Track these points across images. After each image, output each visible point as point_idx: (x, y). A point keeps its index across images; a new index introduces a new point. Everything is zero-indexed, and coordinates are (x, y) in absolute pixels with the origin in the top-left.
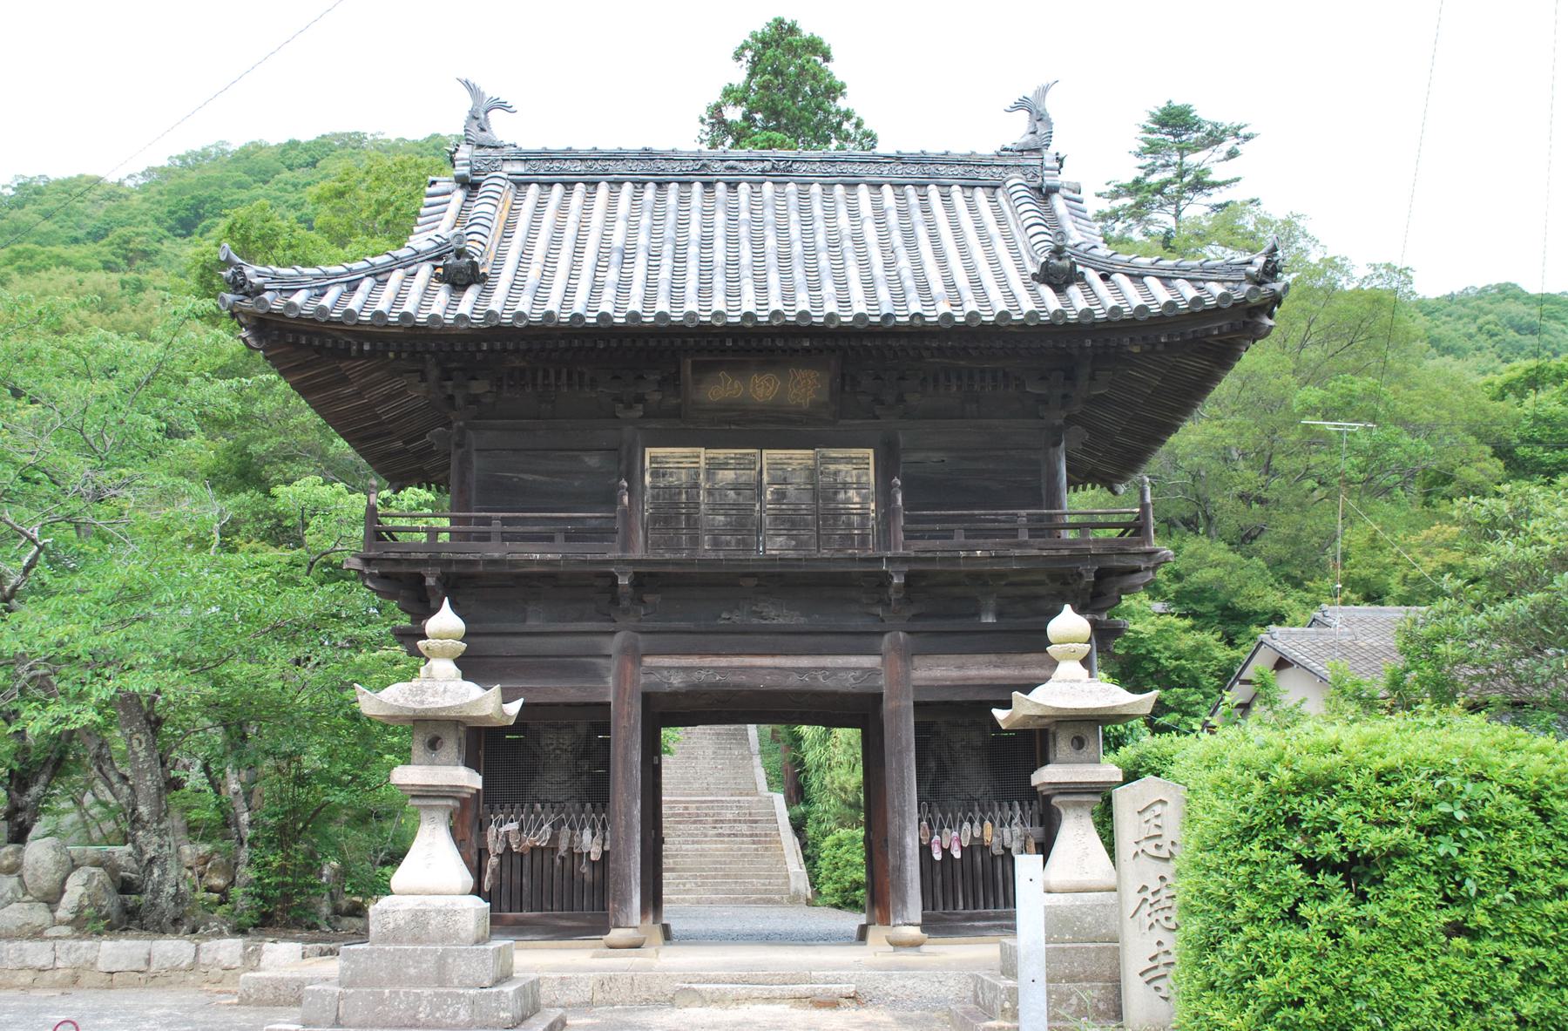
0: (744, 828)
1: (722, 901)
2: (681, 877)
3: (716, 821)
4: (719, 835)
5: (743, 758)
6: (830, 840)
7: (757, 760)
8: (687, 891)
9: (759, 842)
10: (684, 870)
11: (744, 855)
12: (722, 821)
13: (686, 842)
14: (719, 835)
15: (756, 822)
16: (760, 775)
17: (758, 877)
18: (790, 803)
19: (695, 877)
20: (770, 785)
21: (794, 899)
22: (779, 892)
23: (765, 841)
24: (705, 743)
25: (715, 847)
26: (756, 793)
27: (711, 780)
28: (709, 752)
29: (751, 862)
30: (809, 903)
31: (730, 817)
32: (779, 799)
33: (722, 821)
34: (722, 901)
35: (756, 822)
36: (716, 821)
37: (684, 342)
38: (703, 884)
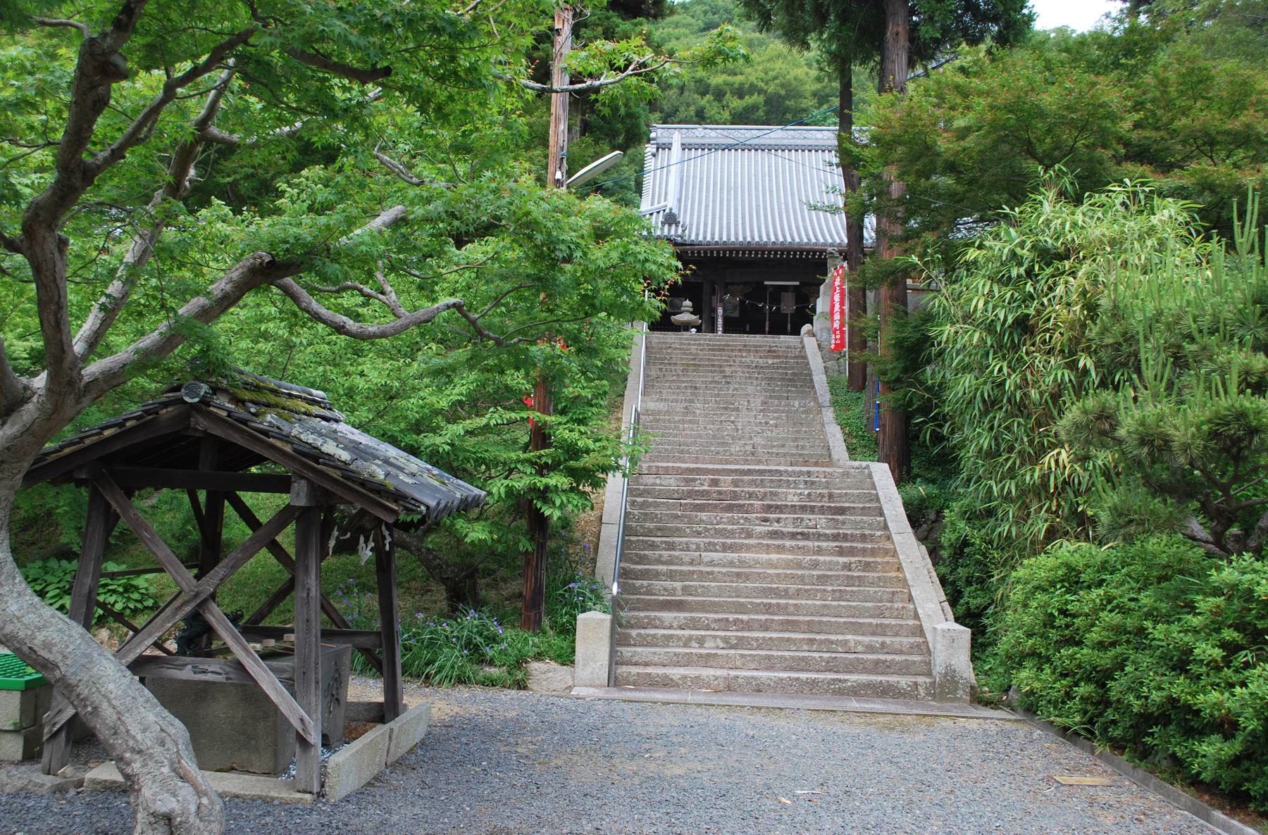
0: (821, 522)
1: (780, 687)
2: (693, 624)
3: (769, 508)
4: (774, 535)
5: (807, 412)
6: (1040, 567)
7: (829, 415)
8: (706, 660)
9: (851, 552)
10: (703, 607)
11: (823, 579)
12: (780, 509)
13: (710, 547)
14: (774, 535)
15: (842, 511)
16: (836, 437)
17: (857, 629)
18: (902, 477)
19: (725, 625)
20: (852, 450)
21: (945, 689)
22: (905, 669)
23: (865, 546)
24: (750, 389)
25: (768, 560)
26: (830, 463)
27: (758, 440)
28: (757, 402)
29: (840, 595)
30: (978, 700)
31: (793, 500)
32: (882, 473)
33: (780, 509)
34: (780, 687)
35: (842, 511)
36: (769, 508)
37: (715, 483)
38: (741, 643)
